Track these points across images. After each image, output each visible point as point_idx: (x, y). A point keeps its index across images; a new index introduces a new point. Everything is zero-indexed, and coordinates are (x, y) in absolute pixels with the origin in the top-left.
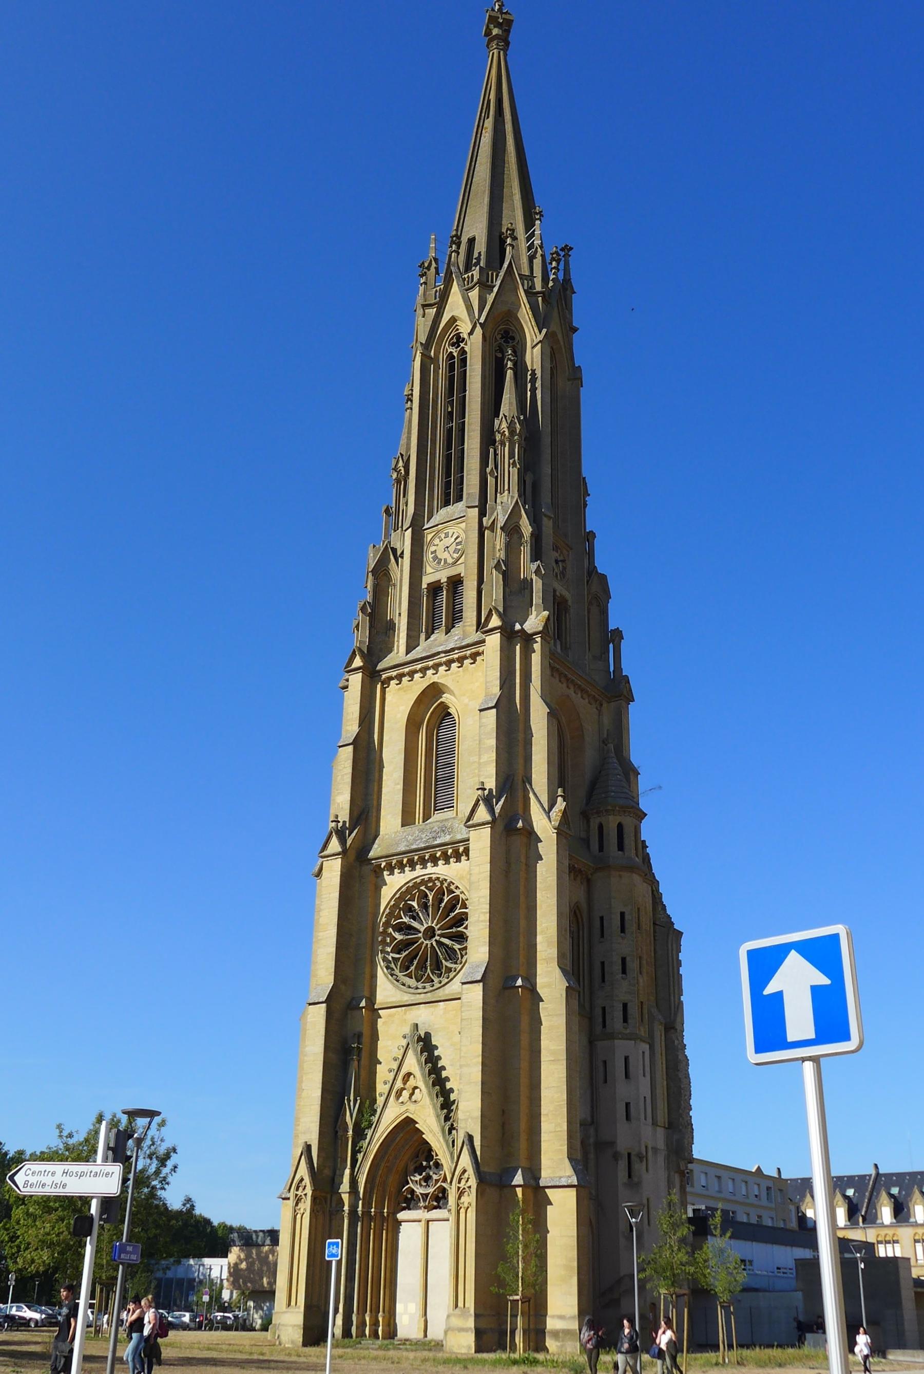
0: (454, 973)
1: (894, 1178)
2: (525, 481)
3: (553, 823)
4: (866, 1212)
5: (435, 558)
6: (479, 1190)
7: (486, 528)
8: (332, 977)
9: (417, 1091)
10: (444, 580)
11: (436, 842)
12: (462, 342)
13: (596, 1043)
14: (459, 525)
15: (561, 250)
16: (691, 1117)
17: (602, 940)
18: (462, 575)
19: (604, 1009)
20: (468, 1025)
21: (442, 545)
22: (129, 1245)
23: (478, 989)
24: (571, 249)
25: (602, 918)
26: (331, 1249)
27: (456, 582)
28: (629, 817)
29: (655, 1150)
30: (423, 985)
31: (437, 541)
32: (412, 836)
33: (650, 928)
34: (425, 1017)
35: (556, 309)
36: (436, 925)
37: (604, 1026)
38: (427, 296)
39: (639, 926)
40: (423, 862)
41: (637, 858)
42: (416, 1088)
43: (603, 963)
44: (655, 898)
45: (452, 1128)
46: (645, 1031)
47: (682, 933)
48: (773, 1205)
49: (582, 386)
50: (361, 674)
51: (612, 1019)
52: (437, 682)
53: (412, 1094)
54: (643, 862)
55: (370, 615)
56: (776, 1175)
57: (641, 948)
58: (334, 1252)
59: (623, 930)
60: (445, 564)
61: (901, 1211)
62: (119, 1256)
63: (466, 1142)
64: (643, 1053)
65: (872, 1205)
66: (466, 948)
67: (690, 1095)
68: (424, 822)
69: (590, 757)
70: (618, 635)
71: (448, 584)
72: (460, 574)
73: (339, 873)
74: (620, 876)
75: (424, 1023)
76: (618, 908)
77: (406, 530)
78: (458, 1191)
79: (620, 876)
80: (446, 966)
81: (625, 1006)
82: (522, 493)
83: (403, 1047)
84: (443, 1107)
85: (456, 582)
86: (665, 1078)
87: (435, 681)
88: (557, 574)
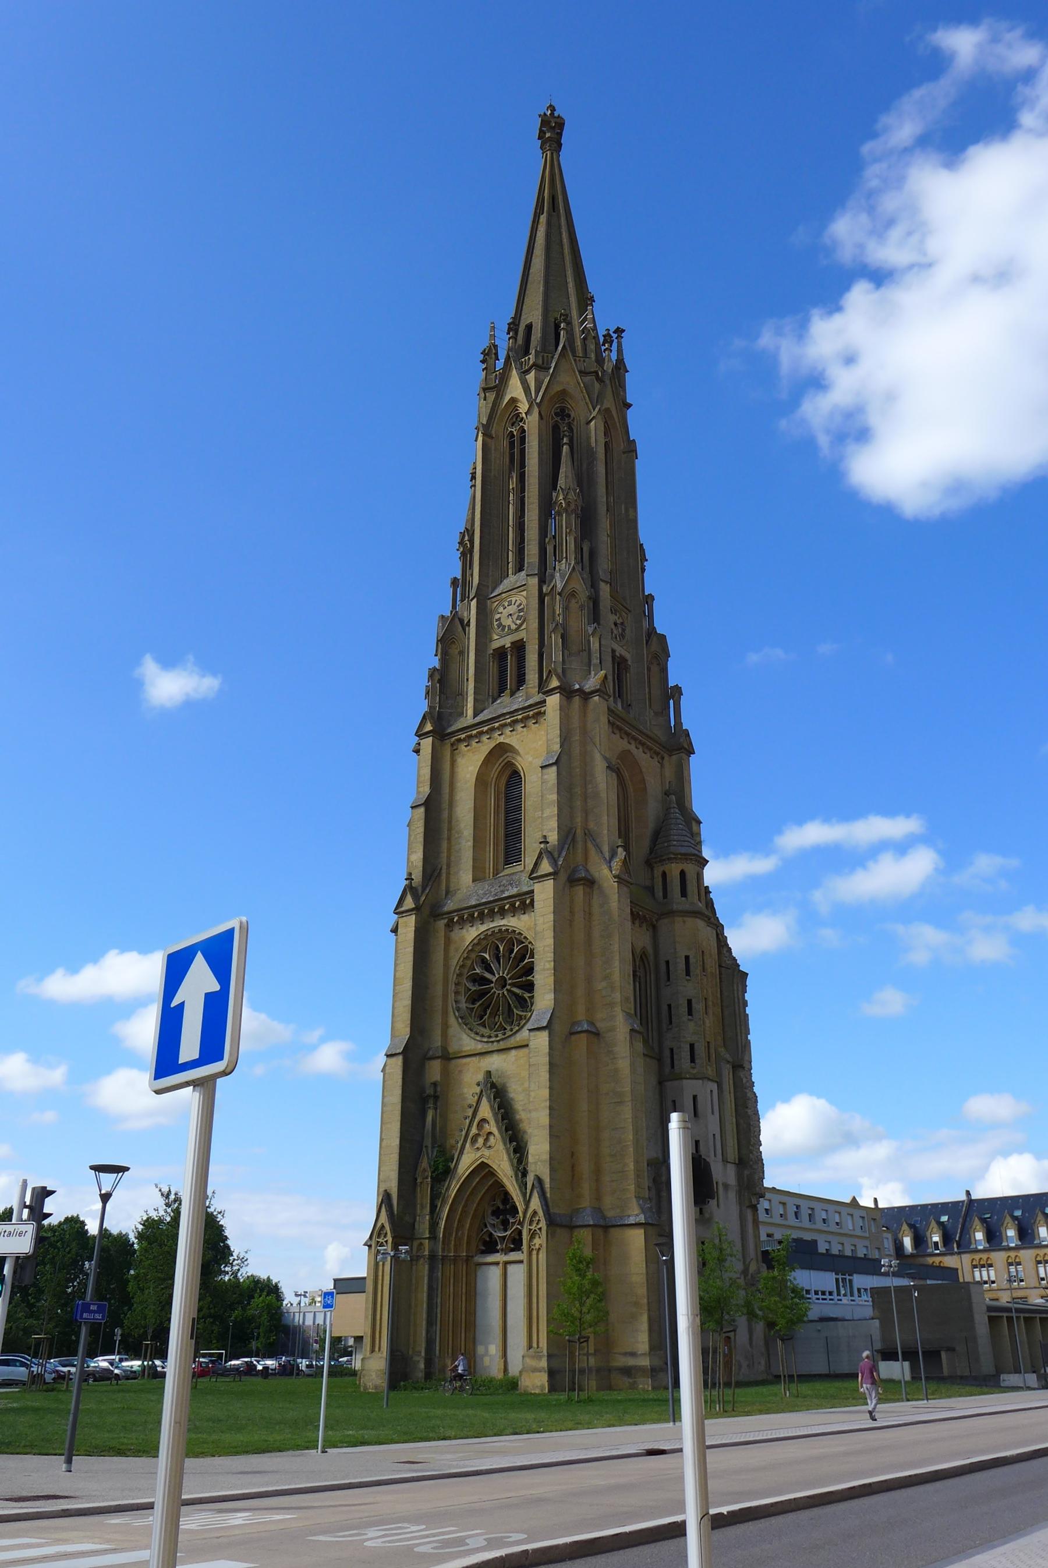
2: (582, 549)
7: (546, 594)
8: (408, 1029)
9: (492, 1138)
10: (508, 645)
11: (504, 896)
13: (666, 1083)
14: (521, 593)
15: (614, 332)
18: (525, 640)
19: (672, 1050)
21: (505, 612)
22: (93, 1304)
23: (544, 1036)
24: (623, 331)
25: (667, 962)
27: (519, 647)
29: (726, 1186)
32: (482, 890)
34: (495, 1063)
35: (609, 386)
36: (507, 975)
37: (673, 1066)
40: (492, 915)
43: (669, 1006)
44: (720, 941)
46: (712, 1070)
47: (747, 974)
48: (868, 1235)
49: (637, 458)
50: (431, 738)
53: (486, 1140)
57: (707, 990)
58: (329, 1302)
59: (688, 973)
61: (1026, 1235)
62: (82, 1315)
64: (711, 1091)
65: (966, 1231)
67: (760, 1131)
69: (652, 809)
70: (677, 691)
71: (512, 648)
73: (414, 928)
75: (497, 1070)
78: (530, 1232)
79: (684, 922)
81: (692, 1046)
84: (515, 1151)
85: (519, 647)
86: (734, 1115)
87: (501, 741)
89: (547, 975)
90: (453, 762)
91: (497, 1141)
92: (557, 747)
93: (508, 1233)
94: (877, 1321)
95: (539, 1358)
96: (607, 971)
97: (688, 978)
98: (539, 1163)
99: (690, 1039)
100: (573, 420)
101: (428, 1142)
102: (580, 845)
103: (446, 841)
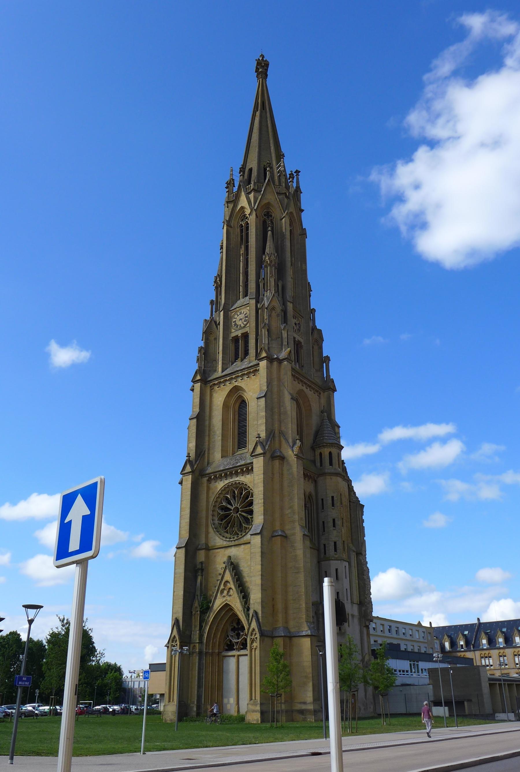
0: (248, 530)
1: (500, 624)
3: (294, 453)
4: (474, 642)
5: (236, 324)
6: (261, 640)
8: (188, 534)
9: (231, 591)
10: (240, 335)
11: (238, 465)
12: (246, 219)
14: (247, 308)
15: (294, 173)
16: (371, 598)
17: (323, 511)
19: (325, 545)
21: (238, 318)
22: (24, 677)
25: (322, 500)
26: (145, 674)
27: (246, 336)
28: (334, 449)
29: (353, 616)
30: (233, 536)
31: (236, 316)
33: (347, 504)
34: (233, 552)
35: (292, 201)
37: (325, 554)
38: (229, 197)
39: (341, 503)
40: (231, 475)
41: (339, 469)
43: (323, 522)
44: (350, 489)
46: (346, 556)
49: (307, 238)
52: (237, 386)
53: (228, 592)
54: (343, 471)
55: (204, 354)
56: (429, 626)
57: (343, 514)
58: (147, 676)
60: (240, 327)
61: (509, 641)
63: (254, 615)
65: (477, 639)
66: (253, 517)
67: (370, 587)
68: (232, 455)
69: (315, 420)
70: (328, 359)
72: (247, 332)
73: (191, 482)
74: (331, 479)
75: (234, 556)
76: (330, 495)
77: (221, 312)
78: (251, 640)
80: (244, 526)
81: (335, 543)
82: (277, 291)
85: (246, 336)
88: (296, 330)
89: (260, 506)
91: (234, 592)
93: (240, 640)
95: (256, 705)
97: (333, 507)
99: (334, 539)
100: (274, 218)
101: (198, 593)
102: (277, 439)
103: (207, 437)
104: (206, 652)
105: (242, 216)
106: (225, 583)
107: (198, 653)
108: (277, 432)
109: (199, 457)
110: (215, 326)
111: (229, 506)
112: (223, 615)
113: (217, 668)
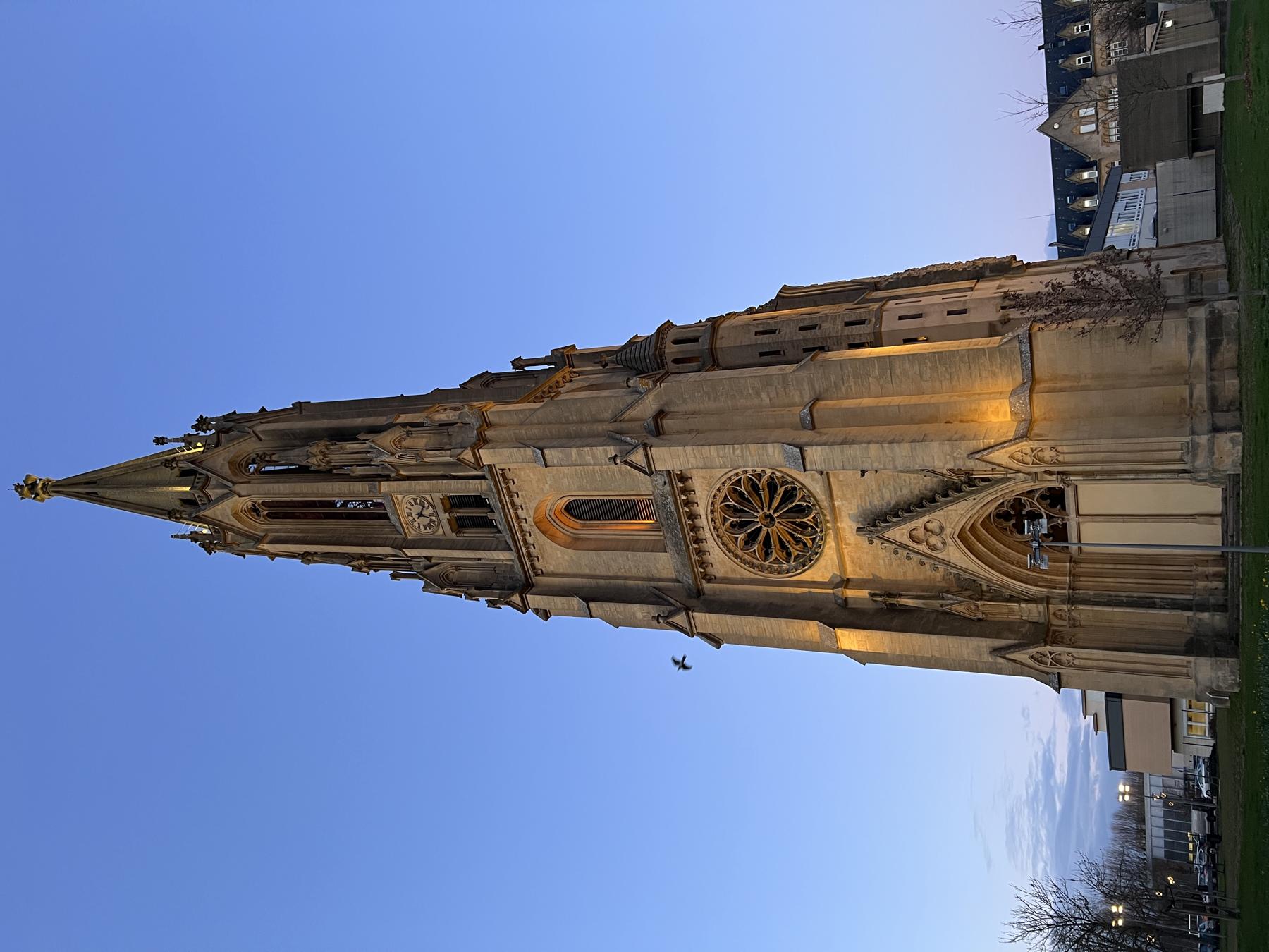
9: (930, 526)
10: (447, 515)
17: (782, 353)
20: (849, 462)
42: (925, 528)
45: (970, 482)
50: (527, 596)
51: (860, 335)
70: (517, 363)
74: (722, 338)
81: (847, 324)
83: (882, 543)
87: (532, 520)
89: (748, 453)
90: (554, 575)
91: (933, 519)
92: (529, 451)
93: (1043, 512)
94: (1158, 165)
96: (750, 392)
98: (955, 454)
99: (840, 325)
101: (936, 604)
102: (624, 425)
103: (627, 582)
104: (1070, 588)
105: (251, 515)
106: (915, 541)
107: (1073, 605)
108: (611, 427)
109: (663, 599)
110: (435, 569)
111: (762, 536)
112: (985, 547)
113: (1106, 566)
